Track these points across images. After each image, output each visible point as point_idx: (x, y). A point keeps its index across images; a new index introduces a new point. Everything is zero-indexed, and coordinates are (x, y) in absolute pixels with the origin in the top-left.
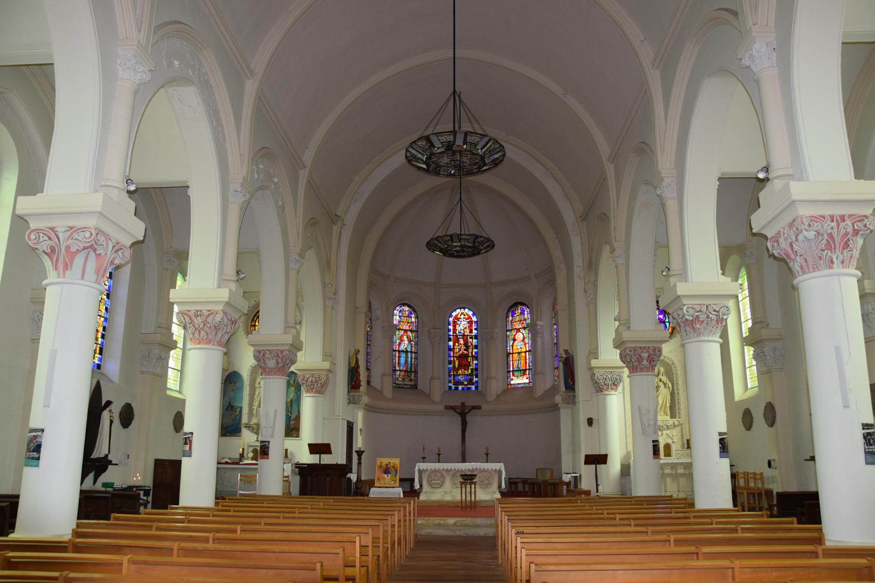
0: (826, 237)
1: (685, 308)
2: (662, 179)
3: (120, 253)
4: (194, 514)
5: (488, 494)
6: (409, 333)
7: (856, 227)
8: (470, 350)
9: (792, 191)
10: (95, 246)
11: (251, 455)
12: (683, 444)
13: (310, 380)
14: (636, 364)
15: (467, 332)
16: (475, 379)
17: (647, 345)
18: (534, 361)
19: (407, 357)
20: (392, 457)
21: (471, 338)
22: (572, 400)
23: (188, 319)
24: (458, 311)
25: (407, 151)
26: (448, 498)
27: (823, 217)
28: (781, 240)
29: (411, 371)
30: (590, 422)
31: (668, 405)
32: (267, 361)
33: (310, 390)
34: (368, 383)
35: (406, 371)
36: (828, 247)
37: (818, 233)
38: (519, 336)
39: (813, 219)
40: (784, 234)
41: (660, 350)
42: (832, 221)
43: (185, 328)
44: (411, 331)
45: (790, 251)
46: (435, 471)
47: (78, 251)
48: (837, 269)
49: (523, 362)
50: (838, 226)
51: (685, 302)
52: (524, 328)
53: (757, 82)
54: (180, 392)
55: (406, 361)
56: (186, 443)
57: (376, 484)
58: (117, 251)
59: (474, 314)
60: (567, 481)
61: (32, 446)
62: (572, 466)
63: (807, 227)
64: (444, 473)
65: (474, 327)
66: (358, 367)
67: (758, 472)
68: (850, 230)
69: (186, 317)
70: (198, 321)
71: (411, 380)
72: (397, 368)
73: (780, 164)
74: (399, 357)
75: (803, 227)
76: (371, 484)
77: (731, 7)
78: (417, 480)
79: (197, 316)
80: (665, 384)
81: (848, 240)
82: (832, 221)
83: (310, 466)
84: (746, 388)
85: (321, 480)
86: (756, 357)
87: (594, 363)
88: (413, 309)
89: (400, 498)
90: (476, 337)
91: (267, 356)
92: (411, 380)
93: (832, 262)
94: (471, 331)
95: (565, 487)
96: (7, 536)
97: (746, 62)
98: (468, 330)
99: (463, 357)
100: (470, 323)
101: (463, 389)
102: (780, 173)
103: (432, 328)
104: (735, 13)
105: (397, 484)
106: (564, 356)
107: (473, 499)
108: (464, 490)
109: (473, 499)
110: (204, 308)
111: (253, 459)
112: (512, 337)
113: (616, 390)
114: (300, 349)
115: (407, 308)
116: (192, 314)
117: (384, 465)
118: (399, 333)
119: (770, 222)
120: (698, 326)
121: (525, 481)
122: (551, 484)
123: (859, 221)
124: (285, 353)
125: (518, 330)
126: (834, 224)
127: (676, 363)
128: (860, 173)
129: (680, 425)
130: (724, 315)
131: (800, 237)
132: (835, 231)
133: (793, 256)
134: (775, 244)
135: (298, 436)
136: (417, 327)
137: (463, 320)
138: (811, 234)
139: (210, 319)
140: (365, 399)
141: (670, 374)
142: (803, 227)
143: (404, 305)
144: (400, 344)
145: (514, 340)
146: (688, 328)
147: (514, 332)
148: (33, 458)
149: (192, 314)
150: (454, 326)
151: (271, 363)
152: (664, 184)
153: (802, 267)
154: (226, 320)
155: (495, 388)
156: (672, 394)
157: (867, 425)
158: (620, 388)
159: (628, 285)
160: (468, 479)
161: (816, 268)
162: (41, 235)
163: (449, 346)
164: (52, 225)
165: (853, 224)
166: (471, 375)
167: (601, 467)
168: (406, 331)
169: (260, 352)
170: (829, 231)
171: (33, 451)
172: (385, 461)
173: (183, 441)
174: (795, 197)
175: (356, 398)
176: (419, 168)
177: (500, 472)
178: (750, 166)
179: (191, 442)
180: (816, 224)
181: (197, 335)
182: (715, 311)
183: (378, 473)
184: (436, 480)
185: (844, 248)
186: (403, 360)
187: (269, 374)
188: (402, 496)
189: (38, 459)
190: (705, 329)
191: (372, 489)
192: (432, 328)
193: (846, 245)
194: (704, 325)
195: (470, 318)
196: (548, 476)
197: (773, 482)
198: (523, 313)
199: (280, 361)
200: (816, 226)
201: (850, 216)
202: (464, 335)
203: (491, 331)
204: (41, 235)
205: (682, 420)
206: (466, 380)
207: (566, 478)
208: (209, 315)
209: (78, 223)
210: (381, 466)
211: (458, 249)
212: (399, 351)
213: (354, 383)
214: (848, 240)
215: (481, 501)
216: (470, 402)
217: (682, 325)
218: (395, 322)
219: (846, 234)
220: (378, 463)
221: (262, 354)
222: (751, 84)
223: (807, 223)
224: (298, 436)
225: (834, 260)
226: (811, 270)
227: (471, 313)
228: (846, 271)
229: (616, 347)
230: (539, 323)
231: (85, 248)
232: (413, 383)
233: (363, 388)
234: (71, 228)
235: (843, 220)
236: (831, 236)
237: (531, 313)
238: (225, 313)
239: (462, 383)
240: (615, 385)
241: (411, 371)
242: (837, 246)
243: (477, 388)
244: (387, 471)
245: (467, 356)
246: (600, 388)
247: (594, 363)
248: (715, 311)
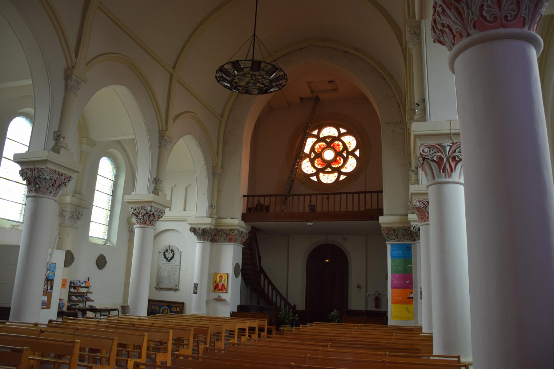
27: (56, 171)
176: (225, 86)
186: (307, 203)
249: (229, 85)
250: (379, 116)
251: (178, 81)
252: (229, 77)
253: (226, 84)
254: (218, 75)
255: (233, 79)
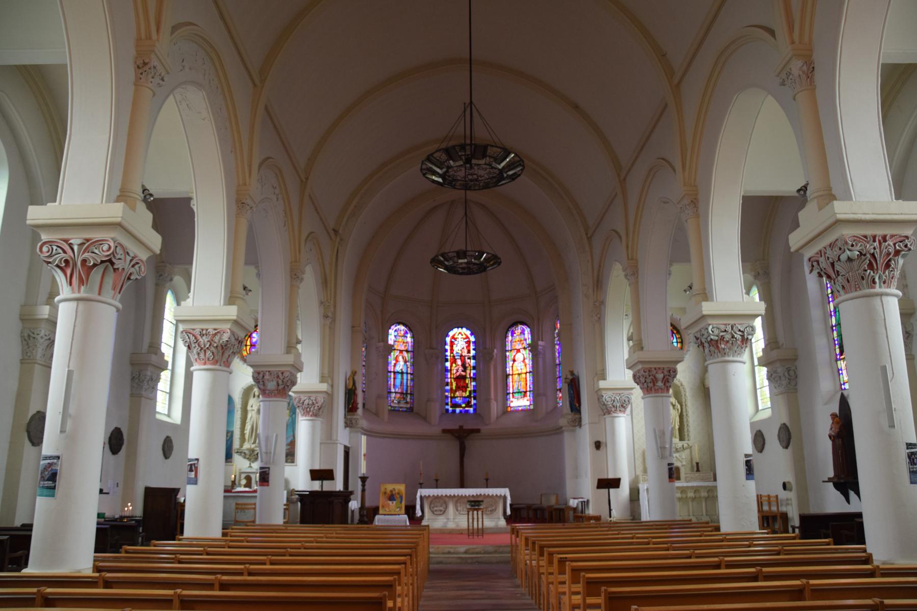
0: (868, 255)
1: (710, 327)
3: (137, 267)
4: (206, 548)
5: (495, 521)
6: (405, 354)
8: (468, 371)
10: (114, 260)
11: (244, 482)
12: (692, 467)
13: (306, 402)
14: (651, 385)
15: (465, 353)
16: (473, 402)
17: (661, 366)
18: (535, 382)
19: (402, 378)
20: (398, 482)
21: (469, 358)
22: (578, 423)
23: (192, 338)
24: (455, 330)
25: (423, 163)
26: (451, 525)
27: (866, 237)
29: (407, 394)
30: (598, 445)
31: (677, 427)
32: (266, 382)
33: (306, 412)
34: (364, 405)
35: (402, 393)
36: (871, 266)
38: (519, 357)
39: (856, 239)
41: (675, 371)
43: (189, 347)
44: (407, 351)
46: (437, 497)
47: (95, 265)
49: (523, 383)
51: (710, 322)
52: (525, 348)
54: (169, 416)
55: (402, 383)
56: (191, 470)
57: (381, 511)
58: (133, 266)
59: (471, 334)
60: (575, 506)
61: (47, 474)
62: (581, 490)
64: (447, 499)
65: (472, 347)
66: (355, 389)
67: (773, 494)
68: (892, 250)
69: (191, 336)
70: (204, 340)
71: (407, 403)
72: (393, 390)
74: (394, 379)
76: (375, 511)
78: (418, 507)
79: (202, 335)
80: (674, 406)
81: (890, 260)
83: (313, 493)
84: (757, 410)
85: (318, 507)
86: (770, 377)
87: (602, 384)
88: (410, 328)
89: (406, 526)
90: (474, 357)
91: (267, 377)
92: (407, 403)
93: (874, 282)
94: (469, 352)
95: (571, 513)
96: (20, 571)
98: (466, 351)
99: (460, 379)
100: (468, 342)
101: (461, 411)
103: (429, 351)
105: (403, 511)
106: (570, 377)
107: (480, 526)
108: (470, 517)
109: (480, 526)
110: (210, 327)
111: (245, 486)
112: (511, 358)
113: (624, 412)
114: (300, 370)
115: (402, 327)
116: (197, 332)
117: (388, 491)
118: (394, 354)
120: (723, 346)
121: (529, 507)
122: (556, 510)
124: (286, 374)
125: (518, 351)
127: (684, 384)
128: (899, 195)
129: (690, 447)
130: (749, 334)
132: (878, 250)
135: (293, 462)
136: (413, 346)
137: (460, 340)
139: (217, 339)
140: (363, 423)
141: (677, 395)
143: (399, 323)
144: (395, 365)
145: (514, 361)
146: (712, 349)
147: (514, 353)
148: (48, 488)
149: (197, 332)
150: (452, 346)
151: (271, 385)
154: (233, 339)
155: (495, 408)
156: (681, 416)
157: (911, 444)
158: (628, 410)
159: (335, 297)
160: (475, 504)
162: (55, 248)
163: (446, 368)
164: (65, 237)
165: (894, 244)
166: (469, 397)
167: (612, 491)
168: (401, 351)
169: (259, 373)
170: (872, 251)
171: (48, 480)
172: (390, 487)
173: (187, 468)
175: (354, 422)
176: (434, 181)
177: (505, 498)
179: (196, 468)
181: (202, 355)
183: (382, 500)
184: (439, 504)
185: (885, 270)
186: (398, 382)
187: (269, 396)
188: (408, 524)
189: (54, 488)
190: (730, 349)
191: (377, 517)
192: (429, 351)
193: (888, 266)
194: (729, 345)
195: (467, 337)
196: (553, 501)
197: (787, 504)
198: (523, 332)
199: (280, 382)
201: (892, 236)
202: (461, 356)
203: (489, 353)
204: (55, 248)
205: (690, 443)
206: (464, 402)
207: (573, 503)
208: (216, 334)
209: (96, 235)
210: (385, 493)
211: (464, 265)
212: (394, 373)
213: (351, 407)
214: (890, 260)
215: (487, 529)
216: (468, 426)
217: (706, 345)
218: (391, 342)
220: (383, 490)
221: (261, 375)
224: (293, 462)
225: (877, 280)
227: (468, 333)
228: (888, 290)
229: (629, 368)
230: (540, 343)
231: (102, 262)
232: (409, 406)
233: (360, 411)
234: (88, 240)
237: (532, 333)
238: (233, 333)
239: (459, 406)
240: (623, 405)
241: (407, 394)
243: (475, 410)
244: (391, 498)
245: (464, 377)
246: (606, 410)
247: (602, 384)
249: (440, 180)
250: (705, 607)
251: (268, 158)
252: (441, 169)
253: (436, 179)
254: (424, 167)
255: (447, 171)
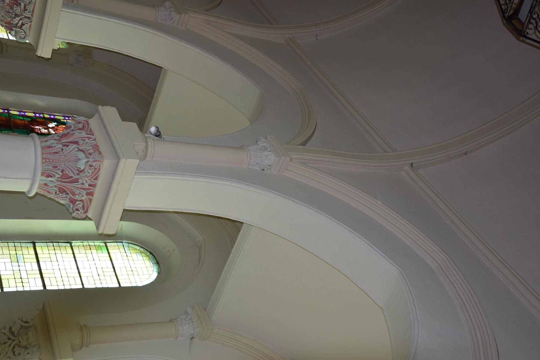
0: (77, 177)
2: (179, 13)
7: (78, 203)
9: (129, 160)
27: (96, 179)
28: (84, 134)
36: (65, 177)
37: (80, 171)
39: (97, 171)
40: (89, 138)
42: (90, 185)
45: (69, 140)
48: (40, 179)
50: (84, 189)
53: (241, 148)
63: (90, 163)
73: (160, 150)
75: (91, 160)
77: (313, 138)
81: (67, 194)
82: (90, 185)
93: (48, 176)
97: (262, 143)
102: (150, 149)
104: (304, 143)
119: (105, 127)
123: (83, 206)
126: (86, 186)
131: (81, 155)
132: (80, 186)
133: (64, 141)
134: (81, 126)
138: (82, 165)
142: (91, 160)
152: (174, 14)
153: (50, 147)
161: (45, 160)
170: (81, 181)
174: (122, 161)
178: (162, 112)
180: (90, 172)
182: (23, 24)
193: (62, 191)
200: (89, 172)
201: (91, 200)
214: (67, 194)
219: (74, 194)
222: (239, 142)
223: (94, 164)
225: (50, 179)
226: (45, 156)
235: (87, 194)
236: (76, 181)
242: (63, 184)
248: (23, 24)
